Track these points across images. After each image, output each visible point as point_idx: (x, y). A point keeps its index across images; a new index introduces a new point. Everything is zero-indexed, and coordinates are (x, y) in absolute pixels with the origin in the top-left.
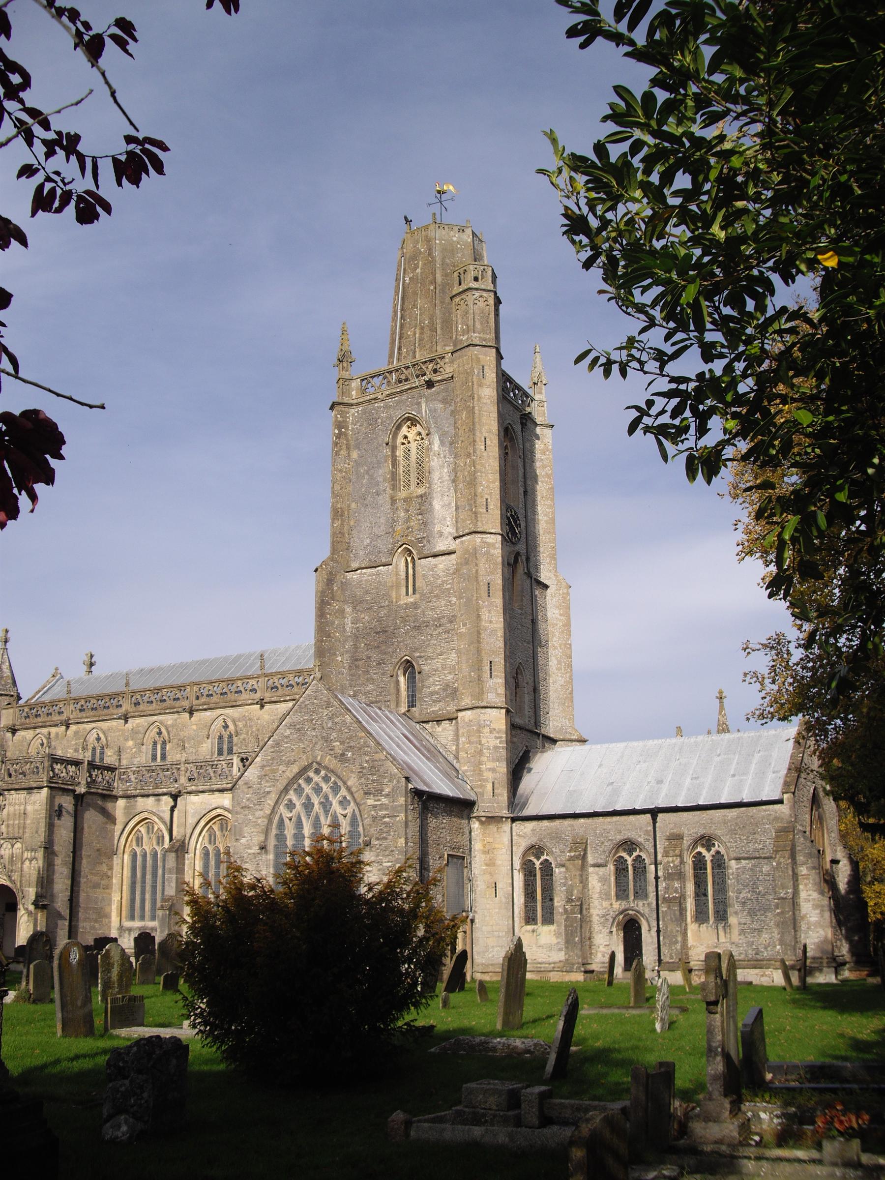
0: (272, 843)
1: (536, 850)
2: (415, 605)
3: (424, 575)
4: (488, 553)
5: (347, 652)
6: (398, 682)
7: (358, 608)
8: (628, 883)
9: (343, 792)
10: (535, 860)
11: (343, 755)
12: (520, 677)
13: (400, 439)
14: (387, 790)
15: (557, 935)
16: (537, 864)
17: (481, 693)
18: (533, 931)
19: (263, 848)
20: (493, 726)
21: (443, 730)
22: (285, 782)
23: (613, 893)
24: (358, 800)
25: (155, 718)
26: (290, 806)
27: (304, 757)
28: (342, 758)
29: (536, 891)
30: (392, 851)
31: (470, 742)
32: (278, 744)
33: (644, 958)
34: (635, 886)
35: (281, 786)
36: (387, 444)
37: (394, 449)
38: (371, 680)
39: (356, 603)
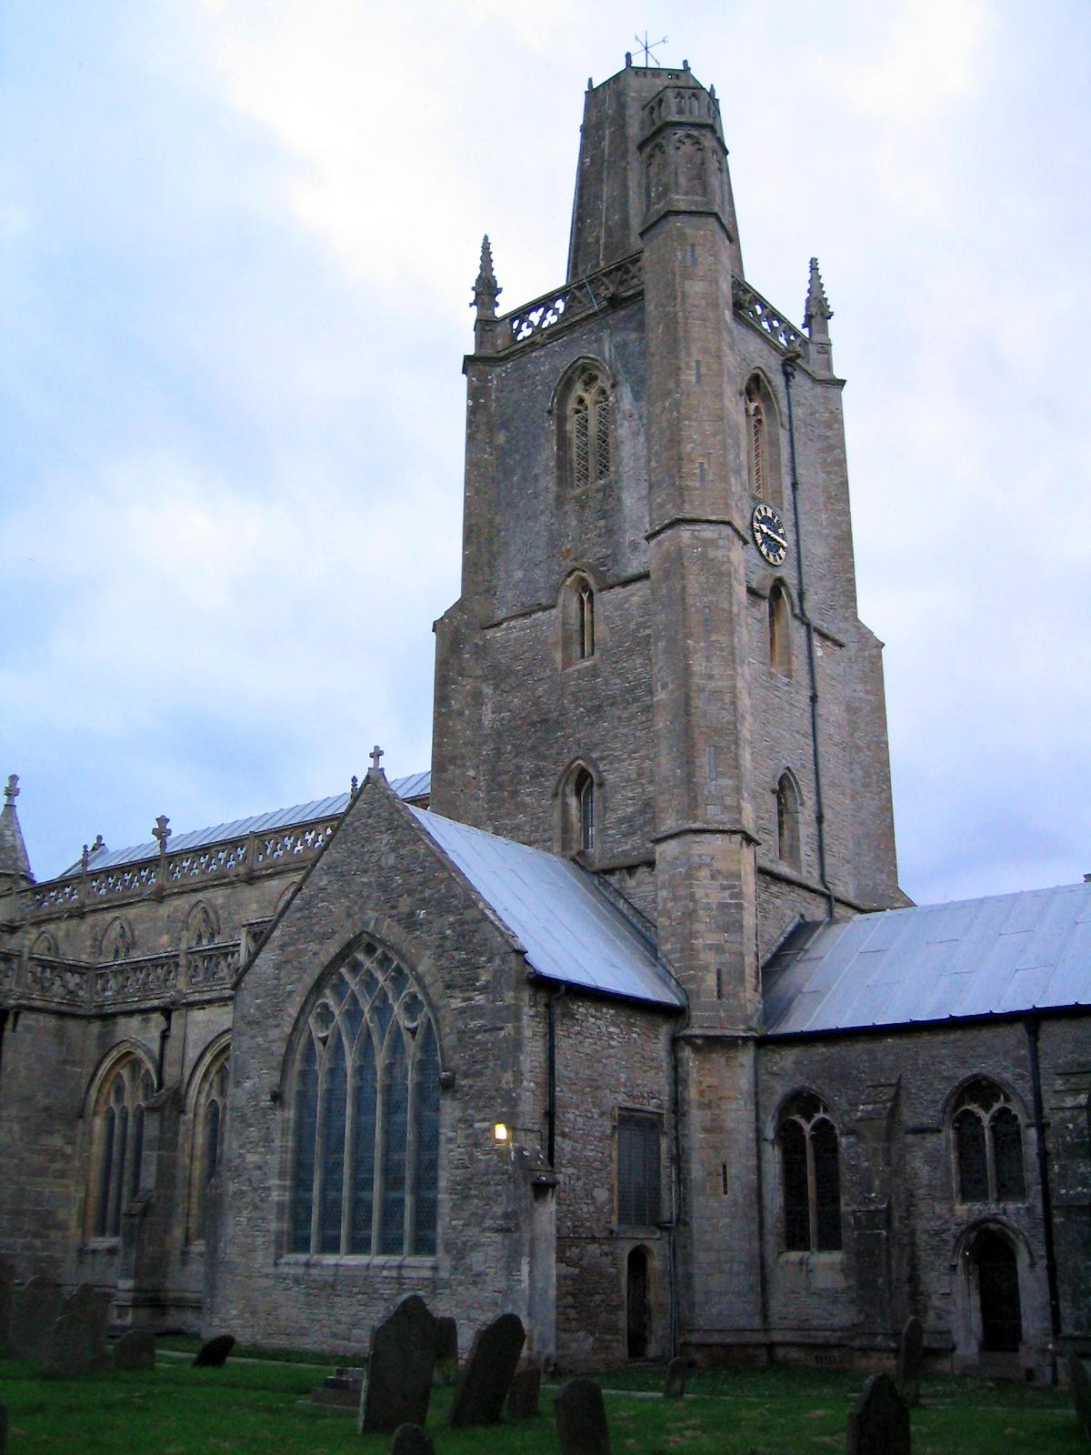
0: (292, 1087)
1: (802, 1101)
2: (594, 672)
3: (607, 618)
4: (703, 556)
5: (484, 762)
6: (565, 806)
7: (502, 686)
8: (984, 1166)
9: (411, 987)
10: (802, 1122)
11: (412, 914)
12: (788, 793)
13: (572, 405)
14: (484, 978)
15: (845, 1270)
16: (807, 1127)
17: (691, 807)
18: (801, 1263)
19: (277, 1097)
20: (718, 865)
21: (639, 884)
22: (317, 972)
23: (955, 1185)
24: (435, 999)
25: (200, 896)
26: (326, 1016)
27: (348, 925)
28: (410, 923)
29: (805, 1182)
30: (491, 1098)
31: (675, 899)
32: (308, 904)
33: (1024, 1324)
34: (998, 1172)
35: (309, 980)
36: (550, 412)
37: (561, 420)
38: (522, 807)
39: (498, 676)
